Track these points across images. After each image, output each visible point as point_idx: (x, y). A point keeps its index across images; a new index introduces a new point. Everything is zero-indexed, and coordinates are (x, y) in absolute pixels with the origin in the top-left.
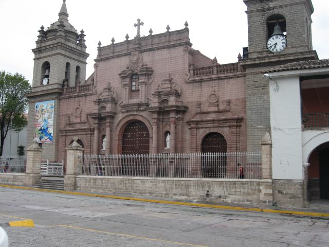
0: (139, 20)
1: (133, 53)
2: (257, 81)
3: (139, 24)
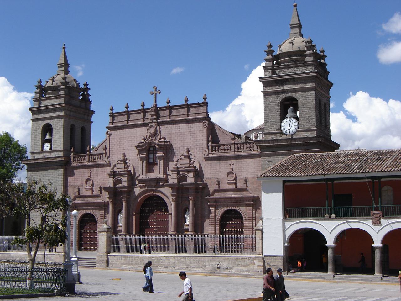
1: (150, 125)
2: (272, 162)
3: (156, 92)
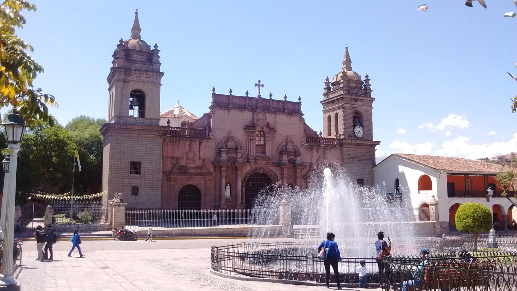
0: (259, 81)
